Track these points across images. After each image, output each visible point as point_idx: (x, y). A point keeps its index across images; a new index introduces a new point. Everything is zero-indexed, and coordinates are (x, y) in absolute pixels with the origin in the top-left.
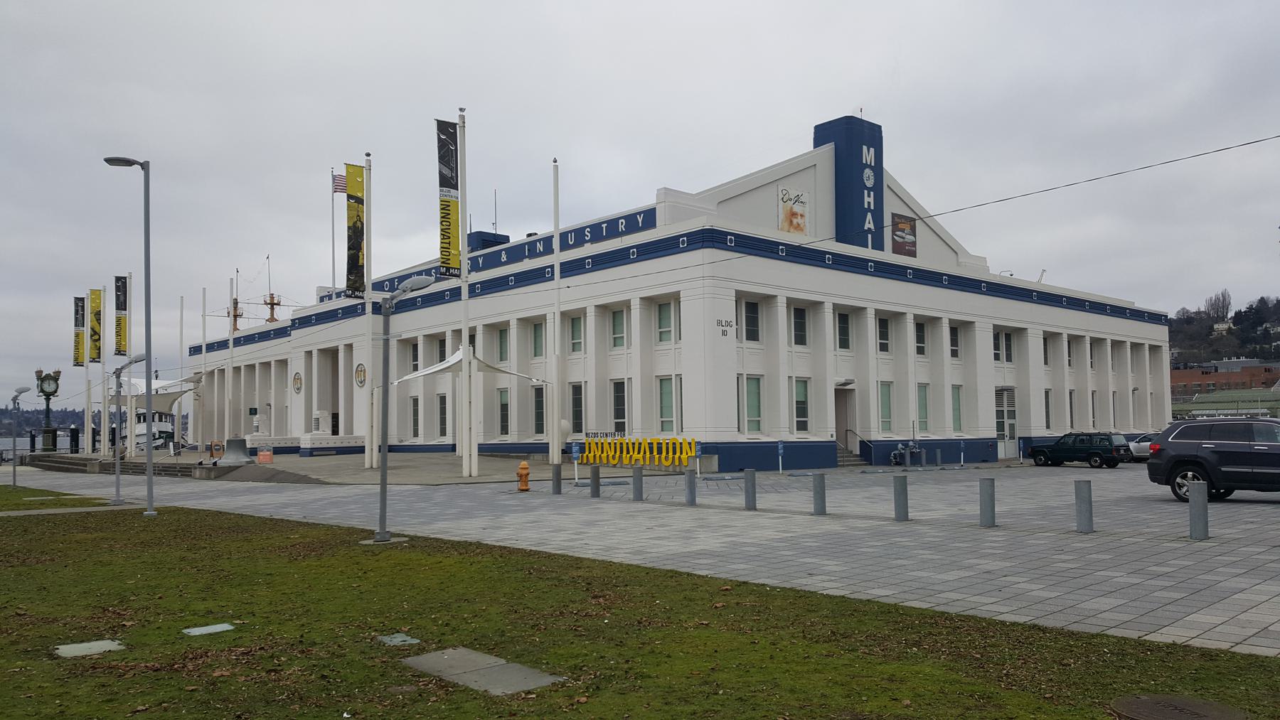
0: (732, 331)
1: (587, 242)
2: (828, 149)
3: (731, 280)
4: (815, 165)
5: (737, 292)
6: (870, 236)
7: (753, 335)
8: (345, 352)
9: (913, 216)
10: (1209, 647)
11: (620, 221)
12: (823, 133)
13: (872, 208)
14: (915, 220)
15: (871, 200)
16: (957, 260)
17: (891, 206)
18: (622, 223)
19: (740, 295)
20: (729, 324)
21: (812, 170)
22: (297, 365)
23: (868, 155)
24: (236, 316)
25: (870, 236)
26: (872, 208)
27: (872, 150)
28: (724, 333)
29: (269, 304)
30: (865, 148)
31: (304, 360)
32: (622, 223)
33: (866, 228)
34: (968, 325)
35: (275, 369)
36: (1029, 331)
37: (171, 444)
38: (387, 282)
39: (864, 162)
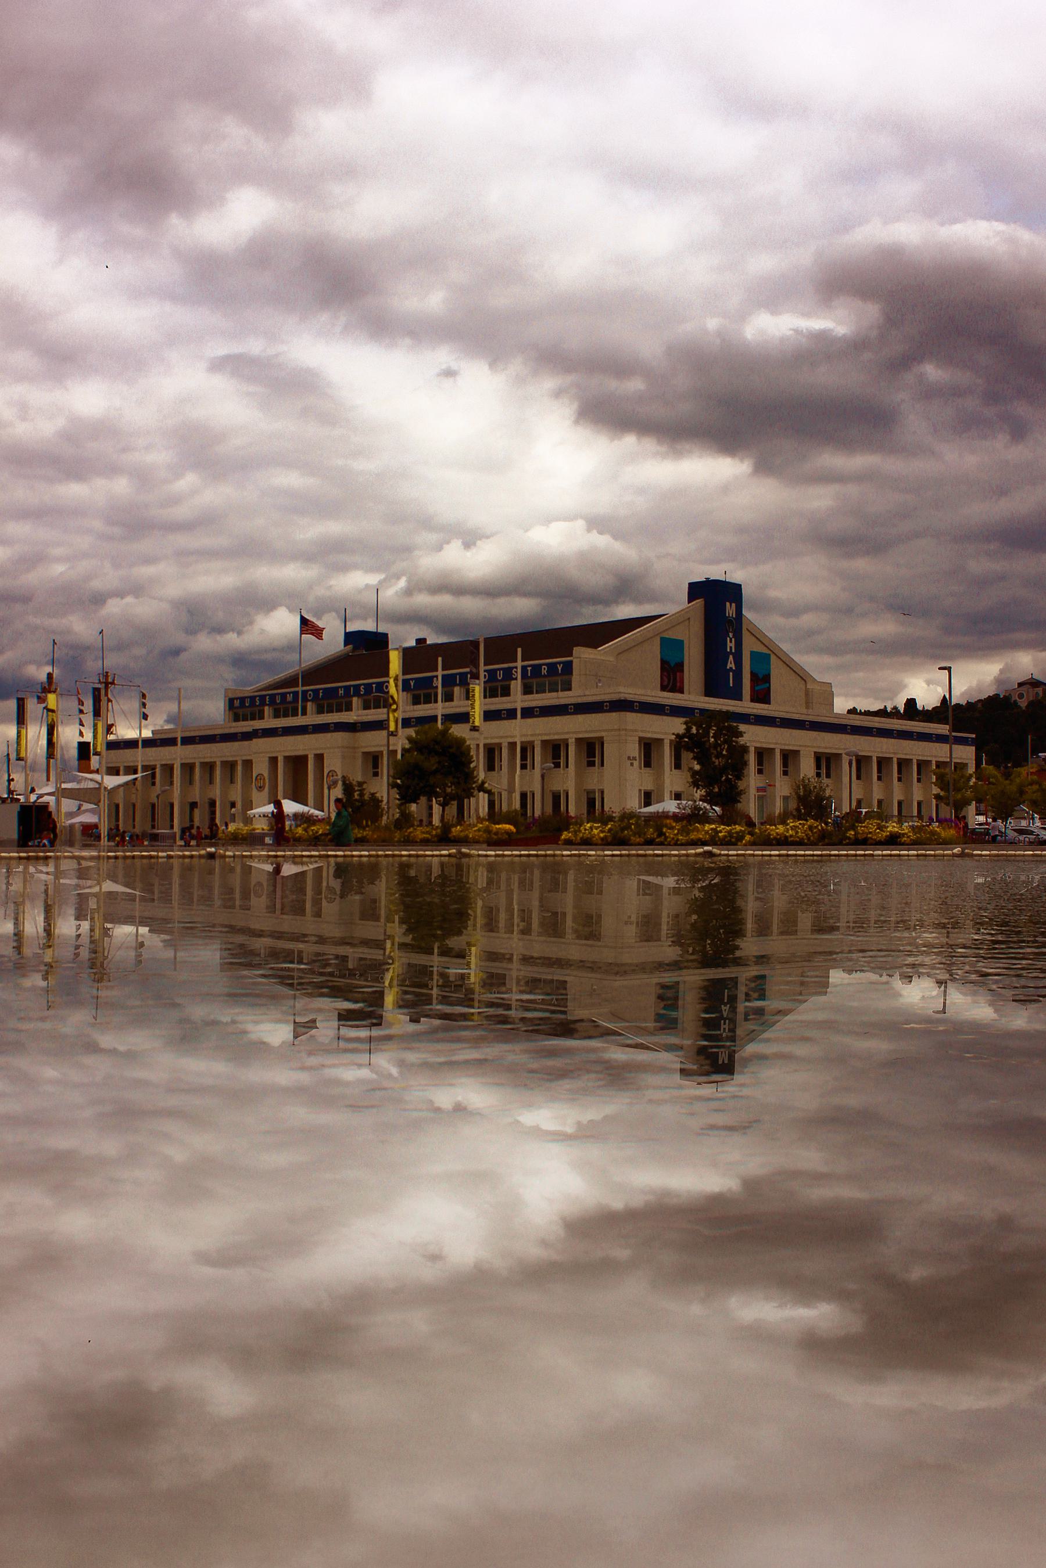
0: (636, 763)
1: (310, 701)
2: (699, 603)
3: (266, 752)
4: (689, 619)
5: (639, 737)
6: (731, 673)
7: (648, 764)
8: (576, 745)
9: (765, 651)
10: (652, 797)
11: (543, 667)
12: (696, 590)
13: (733, 651)
14: (770, 655)
15: (733, 645)
16: (806, 686)
17: (749, 645)
18: (545, 669)
19: (641, 739)
20: (634, 759)
21: (687, 623)
22: (261, 768)
23: (730, 610)
24: (62, 695)
25: (731, 673)
26: (733, 651)
27: (733, 605)
28: (632, 764)
29: (103, 683)
30: (728, 604)
31: (267, 764)
32: (545, 669)
33: (728, 668)
34: (796, 753)
35: (221, 772)
36: (801, 752)
37: (718, 829)
38: (310, 692)
39: (727, 615)
